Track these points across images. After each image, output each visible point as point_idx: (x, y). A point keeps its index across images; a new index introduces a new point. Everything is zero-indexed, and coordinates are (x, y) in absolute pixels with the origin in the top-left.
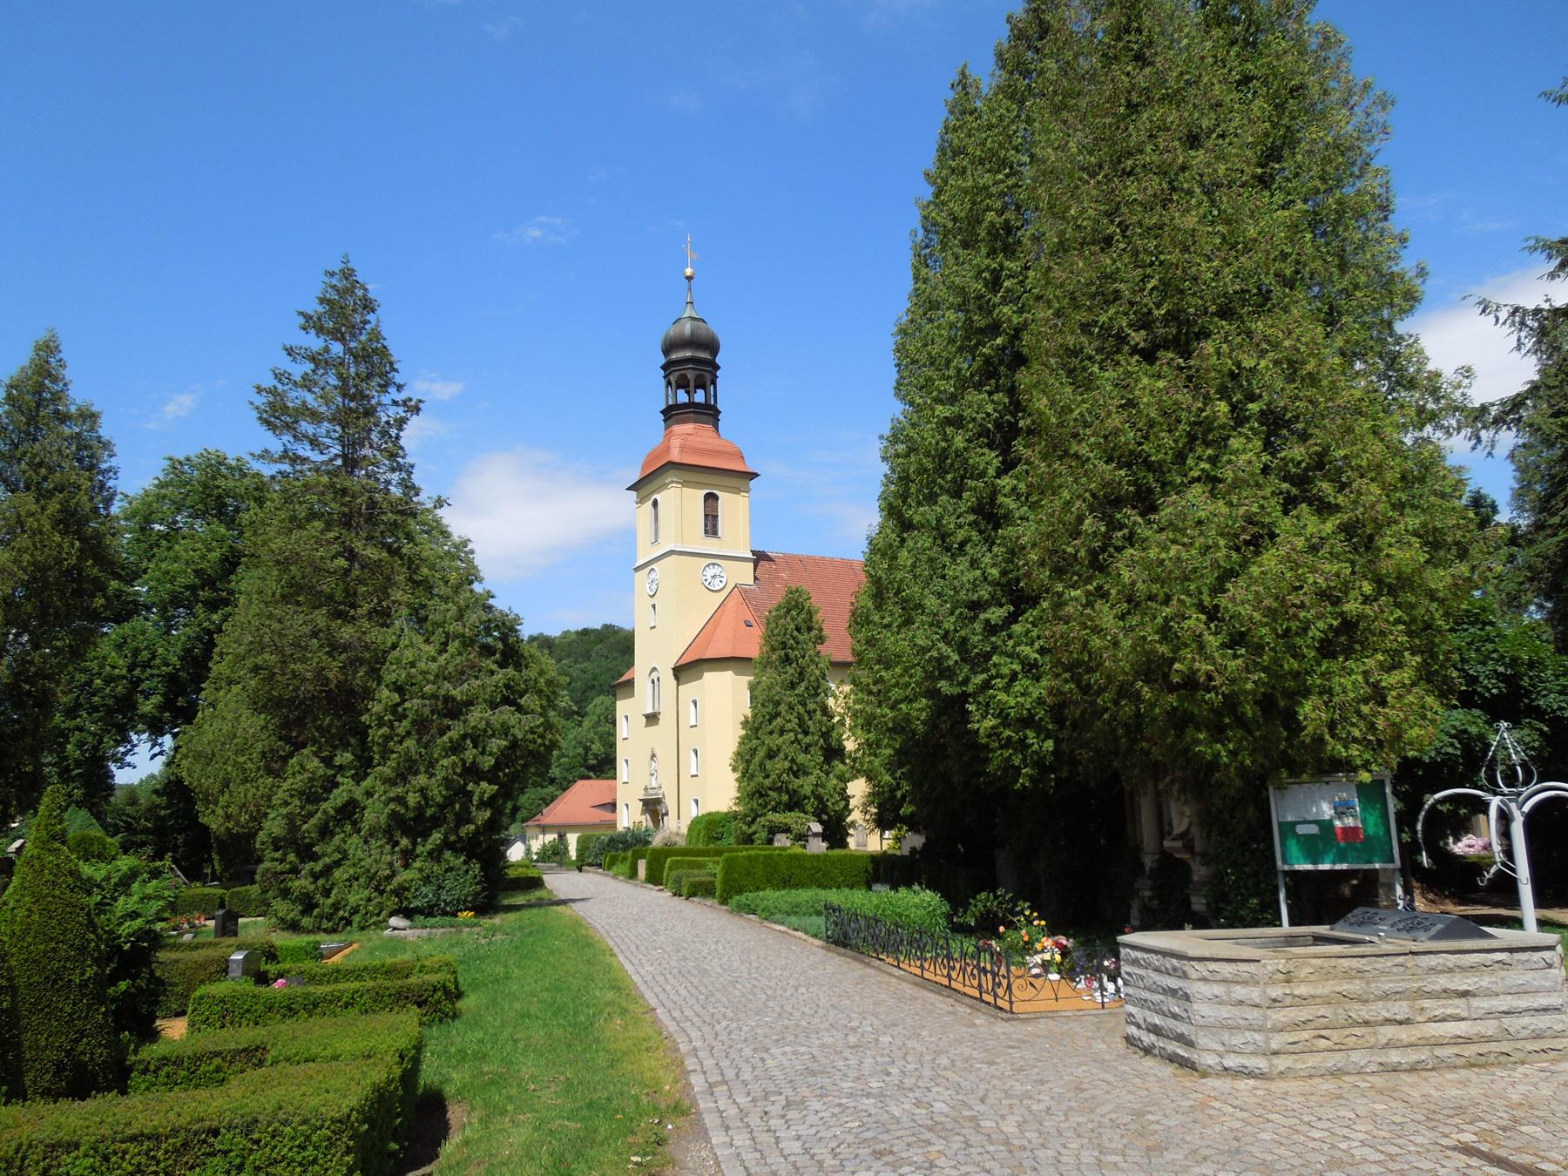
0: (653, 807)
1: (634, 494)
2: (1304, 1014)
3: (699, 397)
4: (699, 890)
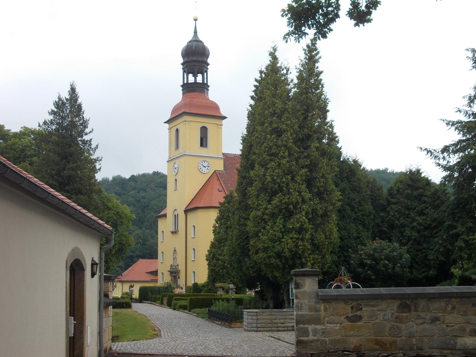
0: (174, 273)
1: (167, 125)
2: (264, 321)
3: (199, 79)
4: (183, 308)
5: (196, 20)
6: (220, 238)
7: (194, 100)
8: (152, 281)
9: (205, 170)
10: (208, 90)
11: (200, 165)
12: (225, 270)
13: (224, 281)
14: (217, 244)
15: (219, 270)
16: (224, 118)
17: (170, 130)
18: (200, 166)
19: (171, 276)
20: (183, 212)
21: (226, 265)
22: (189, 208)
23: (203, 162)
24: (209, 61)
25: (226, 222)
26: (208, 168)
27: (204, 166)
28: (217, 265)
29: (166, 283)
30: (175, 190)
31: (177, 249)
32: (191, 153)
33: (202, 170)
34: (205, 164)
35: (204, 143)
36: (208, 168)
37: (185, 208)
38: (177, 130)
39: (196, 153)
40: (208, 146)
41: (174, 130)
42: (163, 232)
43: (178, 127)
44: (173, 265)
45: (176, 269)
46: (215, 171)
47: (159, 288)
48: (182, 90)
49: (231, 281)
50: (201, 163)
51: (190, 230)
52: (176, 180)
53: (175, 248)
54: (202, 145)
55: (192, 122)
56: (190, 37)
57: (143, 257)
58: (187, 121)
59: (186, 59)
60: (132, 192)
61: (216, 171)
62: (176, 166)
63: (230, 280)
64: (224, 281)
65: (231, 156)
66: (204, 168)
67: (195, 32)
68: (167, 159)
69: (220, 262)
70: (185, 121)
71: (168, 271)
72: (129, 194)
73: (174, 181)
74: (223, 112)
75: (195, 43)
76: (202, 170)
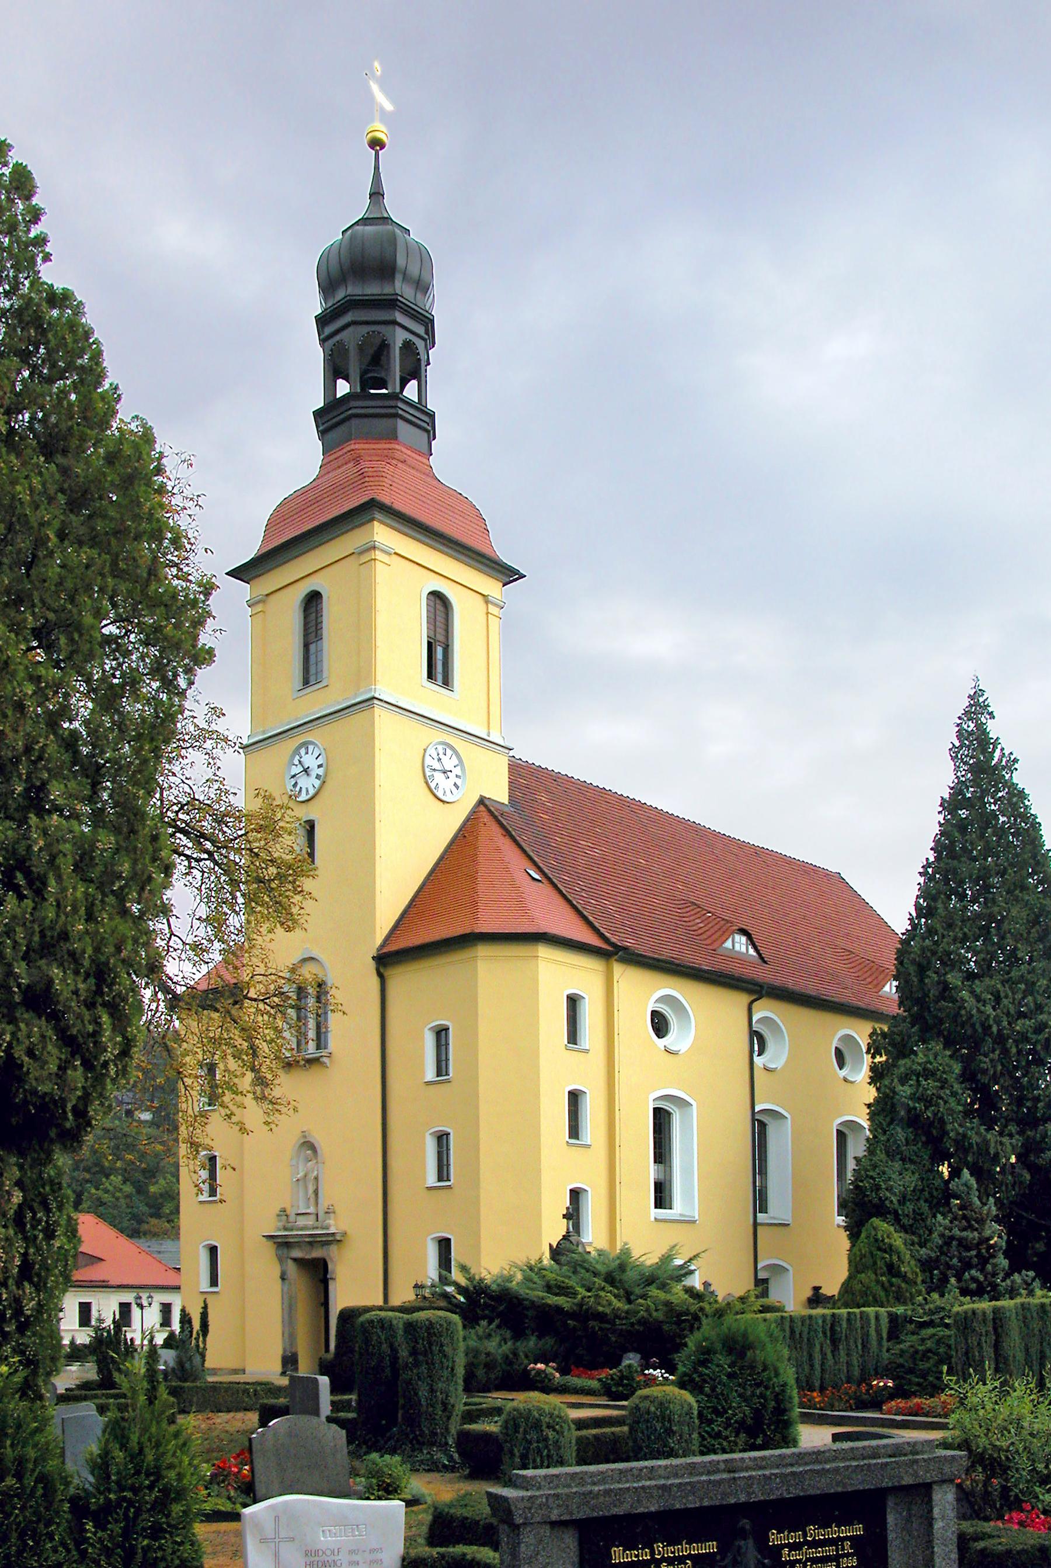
20: (372, 965)
26: (459, 782)
37: (378, 950)
38: (313, 599)
44: (291, 1212)
56: (361, 208)
67: (377, 194)
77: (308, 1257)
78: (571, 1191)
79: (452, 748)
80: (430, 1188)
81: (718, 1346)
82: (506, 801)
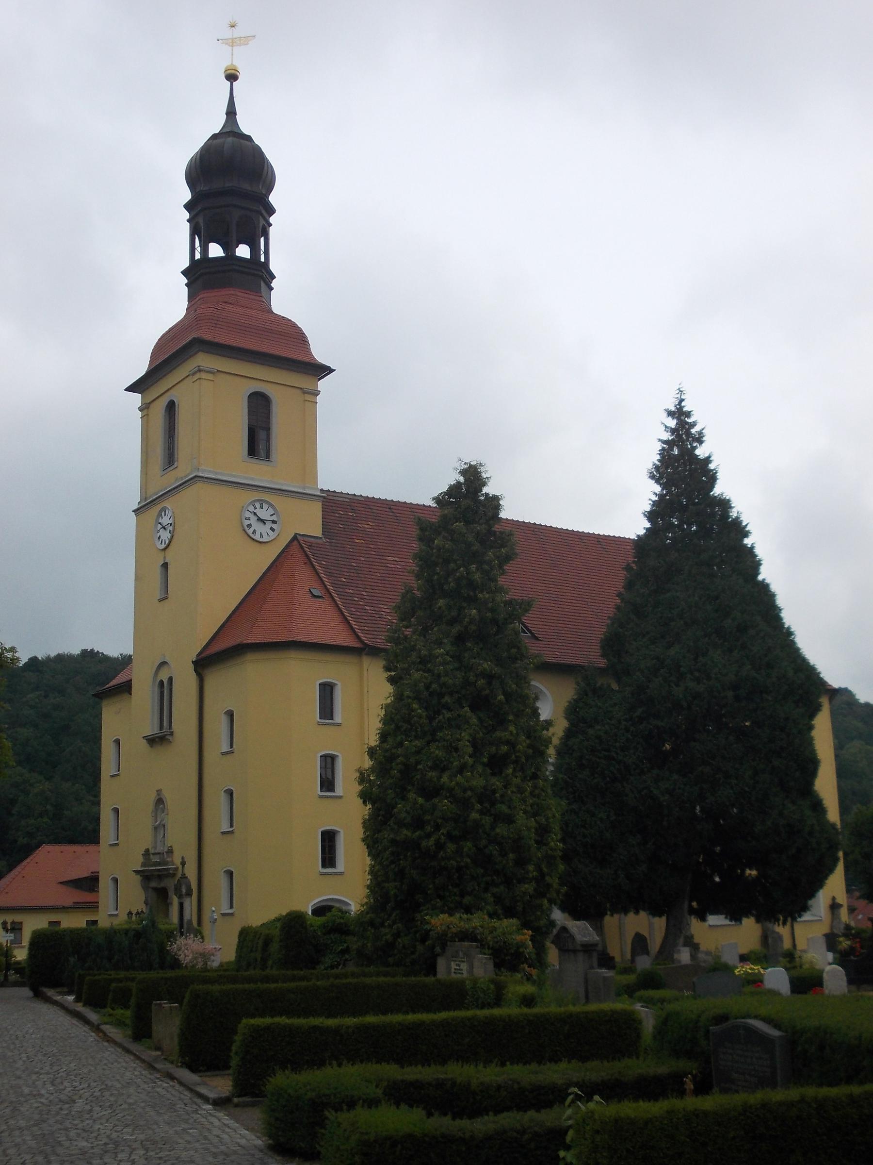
1: (136, 399)
5: (232, 77)
6: (434, 686)
7: (228, 307)
8: (78, 907)
9: (262, 531)
10: (272, 289)
11: (248, 514)
12: (469, 844)
13: (467, 900)
14: (420, 717)
15: (440, 846)
16: (324, 371)
17: (145, 412)
18: (248, 519)
19: (145, 888)
20: (192, 667)
21: (474, 815)
22: (216, 648)
23: (258, 505)
24: (274, 198)
25: (454, 613)
26: (274, 526)
27: (259, 519)
28: (428, 817)
29: (134, 912)
30: (161, 600)
31: (167, 796)
32: (216, 473)
33: (254, 532)
34: (264, 514)
35: (261, 446)
36: (274, 526)
37: (198, 655)
38: (171, 407)
39: (234, 476)
40: (274, 455)
41: (160, 407)
42: (118, 742)
43: (174, 395)
44: (151, 851)
45: (166, 863)
46: (295, 538)
47: (111, 934)
48: (187, 285)
49: (498, 899)
50: (251, 509)
51: (216, 726)
52: (165, 566)
53: (159, 792)
54: (252, 452)
55: (223, 375)
56: (217, 124)
57: (57, 841)
58: (205, 371)
59: (194, 213)
60: (31, 695)
61: (298, 536)
62: (165, 520)
63: (494, 895)
64: (467, 900)
65: (341, 499)
66: (261, 524)
67: (231, 113)
68: (135, 500)
69: (444, 804)
70: (200, 371)
71: (137, 872)
72: (25, 699)
73: (158, 570)
74: (320, 353)
75: (230, 139)
76: (254, 532)
77: (159, 887)
78: (324, 833)
79: (268, 503)
80: (223, 833)
81: (184, 896)
82: (319, 534)
